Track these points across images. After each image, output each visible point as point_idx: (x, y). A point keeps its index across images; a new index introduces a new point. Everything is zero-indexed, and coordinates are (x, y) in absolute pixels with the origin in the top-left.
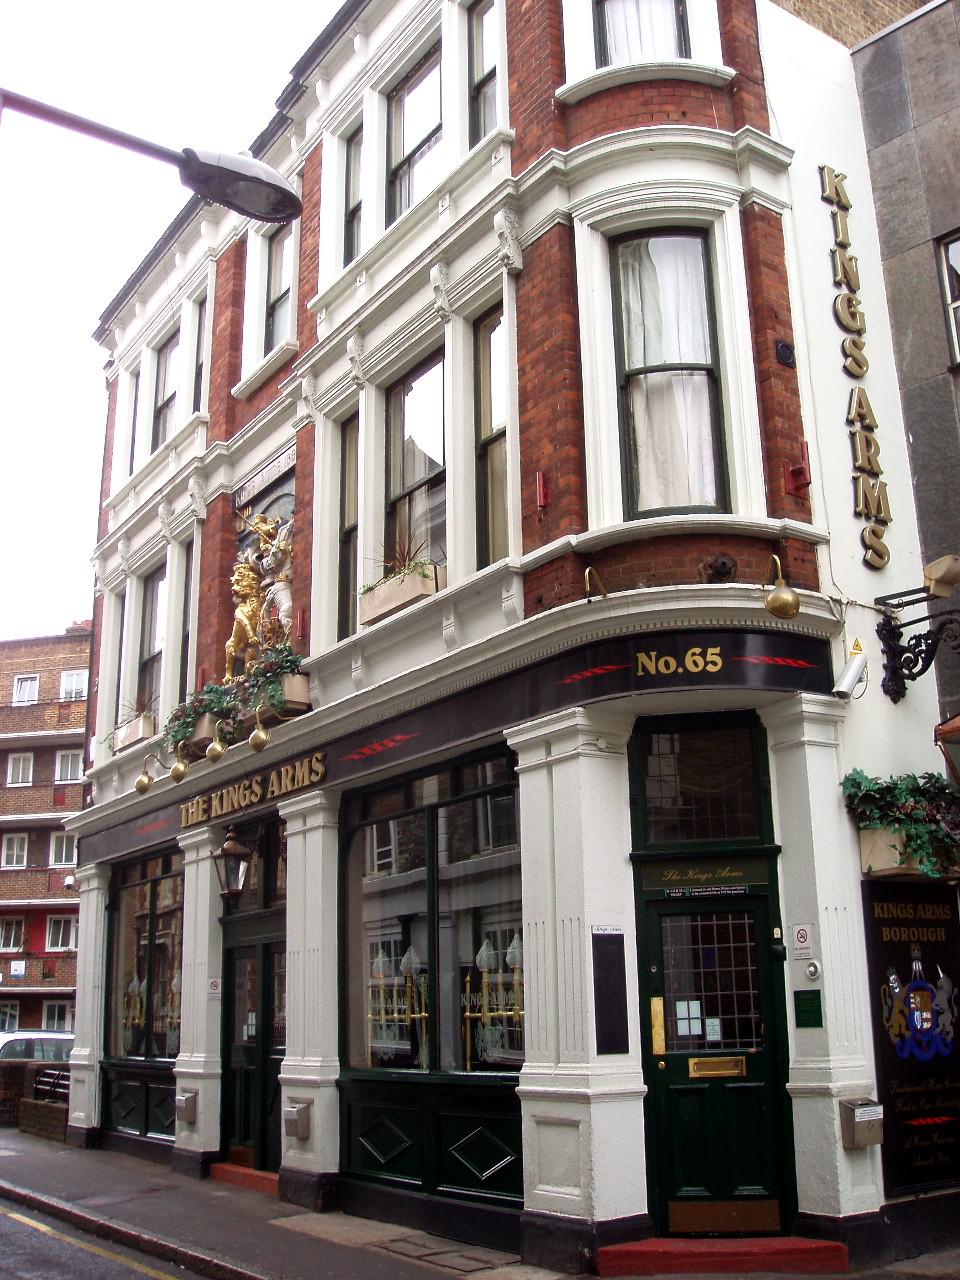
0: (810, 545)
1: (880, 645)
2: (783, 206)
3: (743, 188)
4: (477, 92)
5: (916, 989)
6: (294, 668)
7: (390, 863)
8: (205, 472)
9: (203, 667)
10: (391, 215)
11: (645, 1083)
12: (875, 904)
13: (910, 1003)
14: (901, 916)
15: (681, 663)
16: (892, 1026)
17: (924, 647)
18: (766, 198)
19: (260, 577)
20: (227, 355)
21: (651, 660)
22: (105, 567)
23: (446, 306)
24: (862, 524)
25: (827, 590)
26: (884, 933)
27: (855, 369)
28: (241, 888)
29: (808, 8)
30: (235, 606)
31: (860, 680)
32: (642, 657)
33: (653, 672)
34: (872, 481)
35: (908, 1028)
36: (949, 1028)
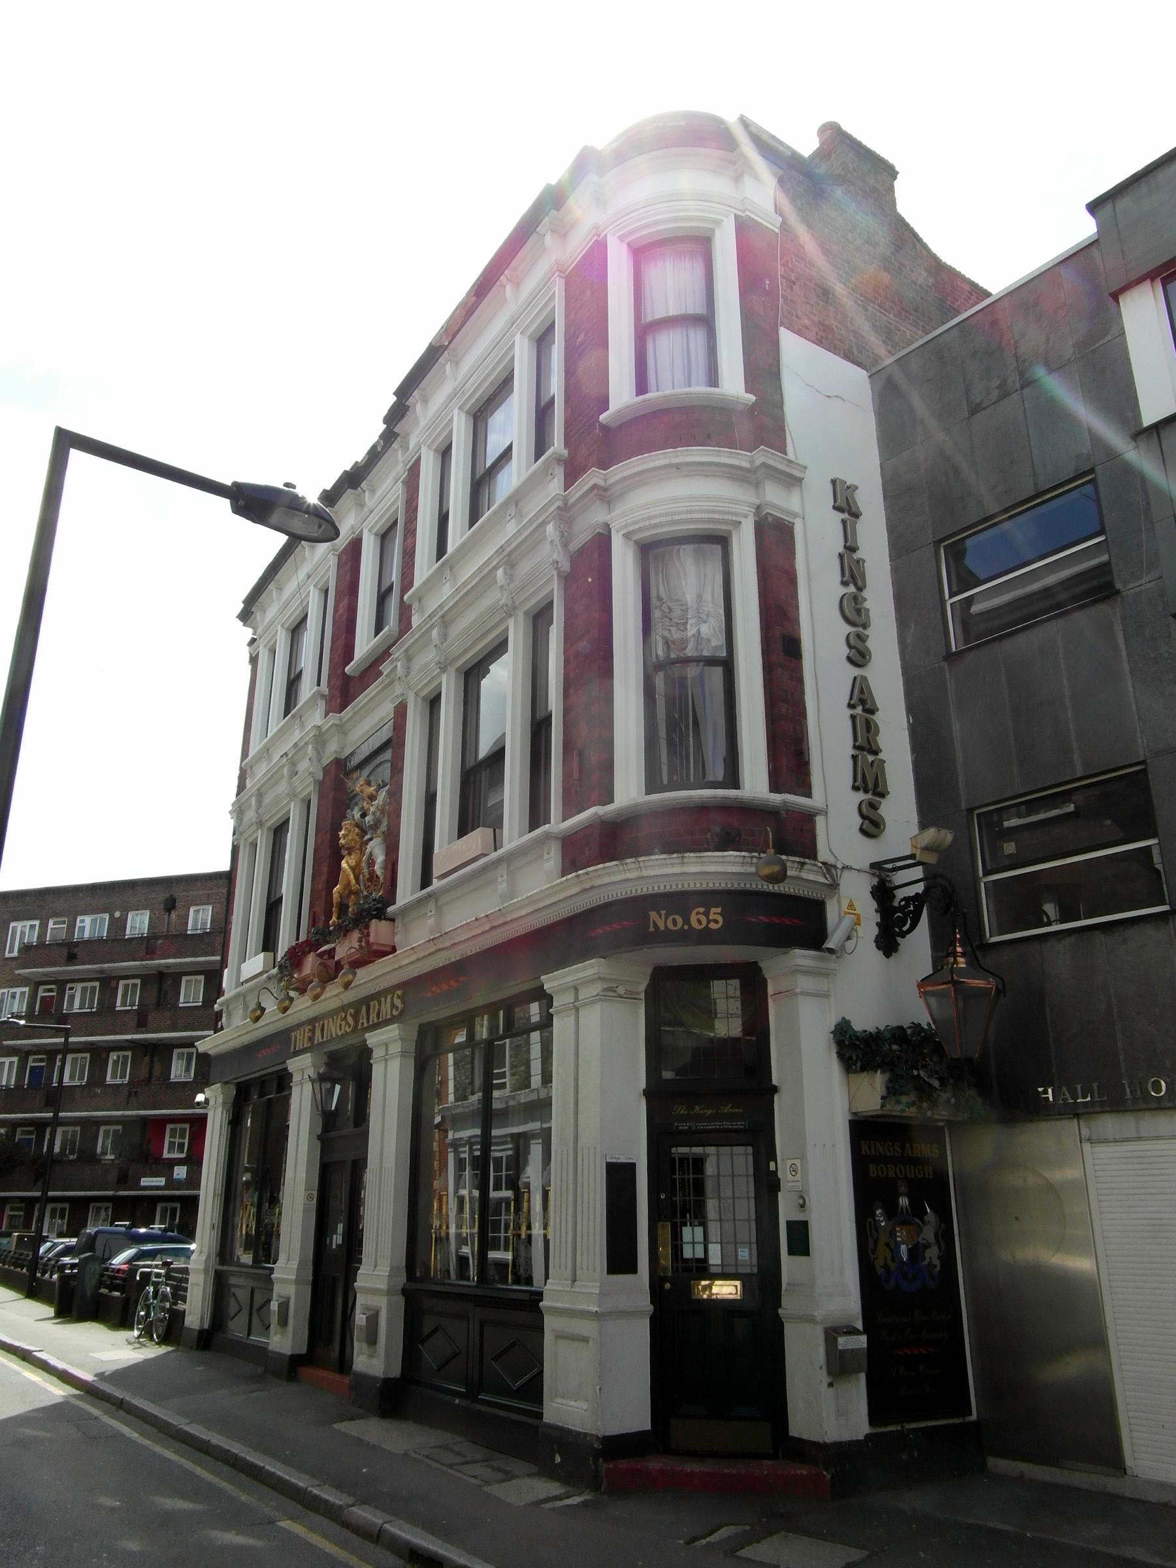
0: (807, 819)
1: (874, 905)
2: (795, 515)
3: (758, 502)
4: (543, 414)
5: (904, 1223)
6: (380, 914)
7: (505, 1083)
8: (320, 739)
9: (314, 910)
10: (474, 517)
11: (652, 1302)
12: (863, 1142)
13: (896, 1237)
14: (888, 1154)
15: (687, 920)
16: (877, 1258)
17: (912, 908)
18: (778, 509)
19: (364, 832)
20: (343, 637)
21: (661, 918)
22: (242, 819)
23: (510, 603)
24: (861, 796)
25: (823, 854)
26: (871, 1169)
27: (859, 656)
28: (333, 1108)
29: (830, 337)
30: (343, 858)
31: (849, 938)
32: (653, 915)
33: (662, 928)
34: (870, 758)
35: (893, 1260)
36: (937, 1262)
